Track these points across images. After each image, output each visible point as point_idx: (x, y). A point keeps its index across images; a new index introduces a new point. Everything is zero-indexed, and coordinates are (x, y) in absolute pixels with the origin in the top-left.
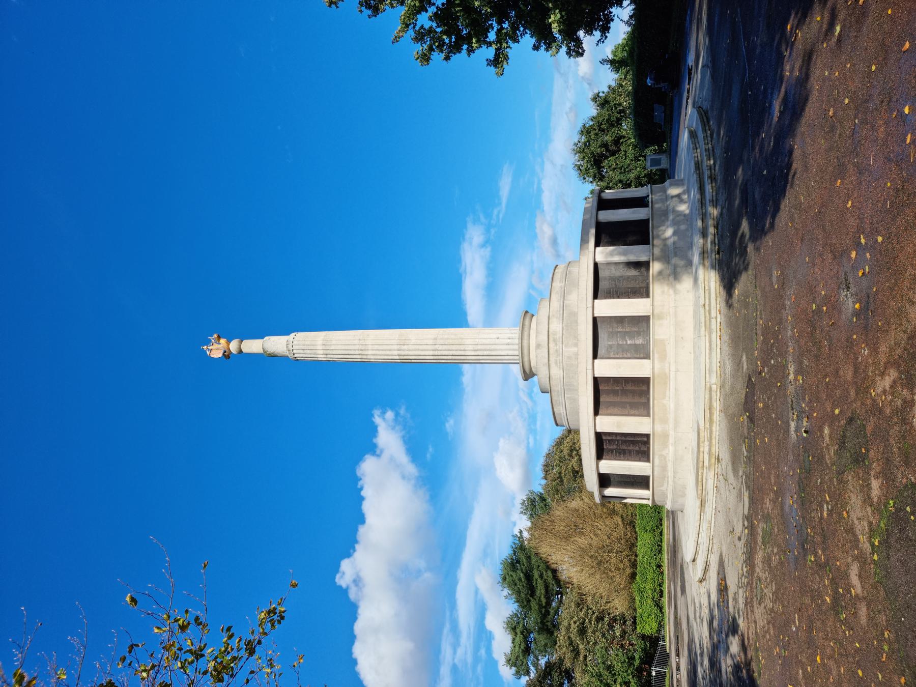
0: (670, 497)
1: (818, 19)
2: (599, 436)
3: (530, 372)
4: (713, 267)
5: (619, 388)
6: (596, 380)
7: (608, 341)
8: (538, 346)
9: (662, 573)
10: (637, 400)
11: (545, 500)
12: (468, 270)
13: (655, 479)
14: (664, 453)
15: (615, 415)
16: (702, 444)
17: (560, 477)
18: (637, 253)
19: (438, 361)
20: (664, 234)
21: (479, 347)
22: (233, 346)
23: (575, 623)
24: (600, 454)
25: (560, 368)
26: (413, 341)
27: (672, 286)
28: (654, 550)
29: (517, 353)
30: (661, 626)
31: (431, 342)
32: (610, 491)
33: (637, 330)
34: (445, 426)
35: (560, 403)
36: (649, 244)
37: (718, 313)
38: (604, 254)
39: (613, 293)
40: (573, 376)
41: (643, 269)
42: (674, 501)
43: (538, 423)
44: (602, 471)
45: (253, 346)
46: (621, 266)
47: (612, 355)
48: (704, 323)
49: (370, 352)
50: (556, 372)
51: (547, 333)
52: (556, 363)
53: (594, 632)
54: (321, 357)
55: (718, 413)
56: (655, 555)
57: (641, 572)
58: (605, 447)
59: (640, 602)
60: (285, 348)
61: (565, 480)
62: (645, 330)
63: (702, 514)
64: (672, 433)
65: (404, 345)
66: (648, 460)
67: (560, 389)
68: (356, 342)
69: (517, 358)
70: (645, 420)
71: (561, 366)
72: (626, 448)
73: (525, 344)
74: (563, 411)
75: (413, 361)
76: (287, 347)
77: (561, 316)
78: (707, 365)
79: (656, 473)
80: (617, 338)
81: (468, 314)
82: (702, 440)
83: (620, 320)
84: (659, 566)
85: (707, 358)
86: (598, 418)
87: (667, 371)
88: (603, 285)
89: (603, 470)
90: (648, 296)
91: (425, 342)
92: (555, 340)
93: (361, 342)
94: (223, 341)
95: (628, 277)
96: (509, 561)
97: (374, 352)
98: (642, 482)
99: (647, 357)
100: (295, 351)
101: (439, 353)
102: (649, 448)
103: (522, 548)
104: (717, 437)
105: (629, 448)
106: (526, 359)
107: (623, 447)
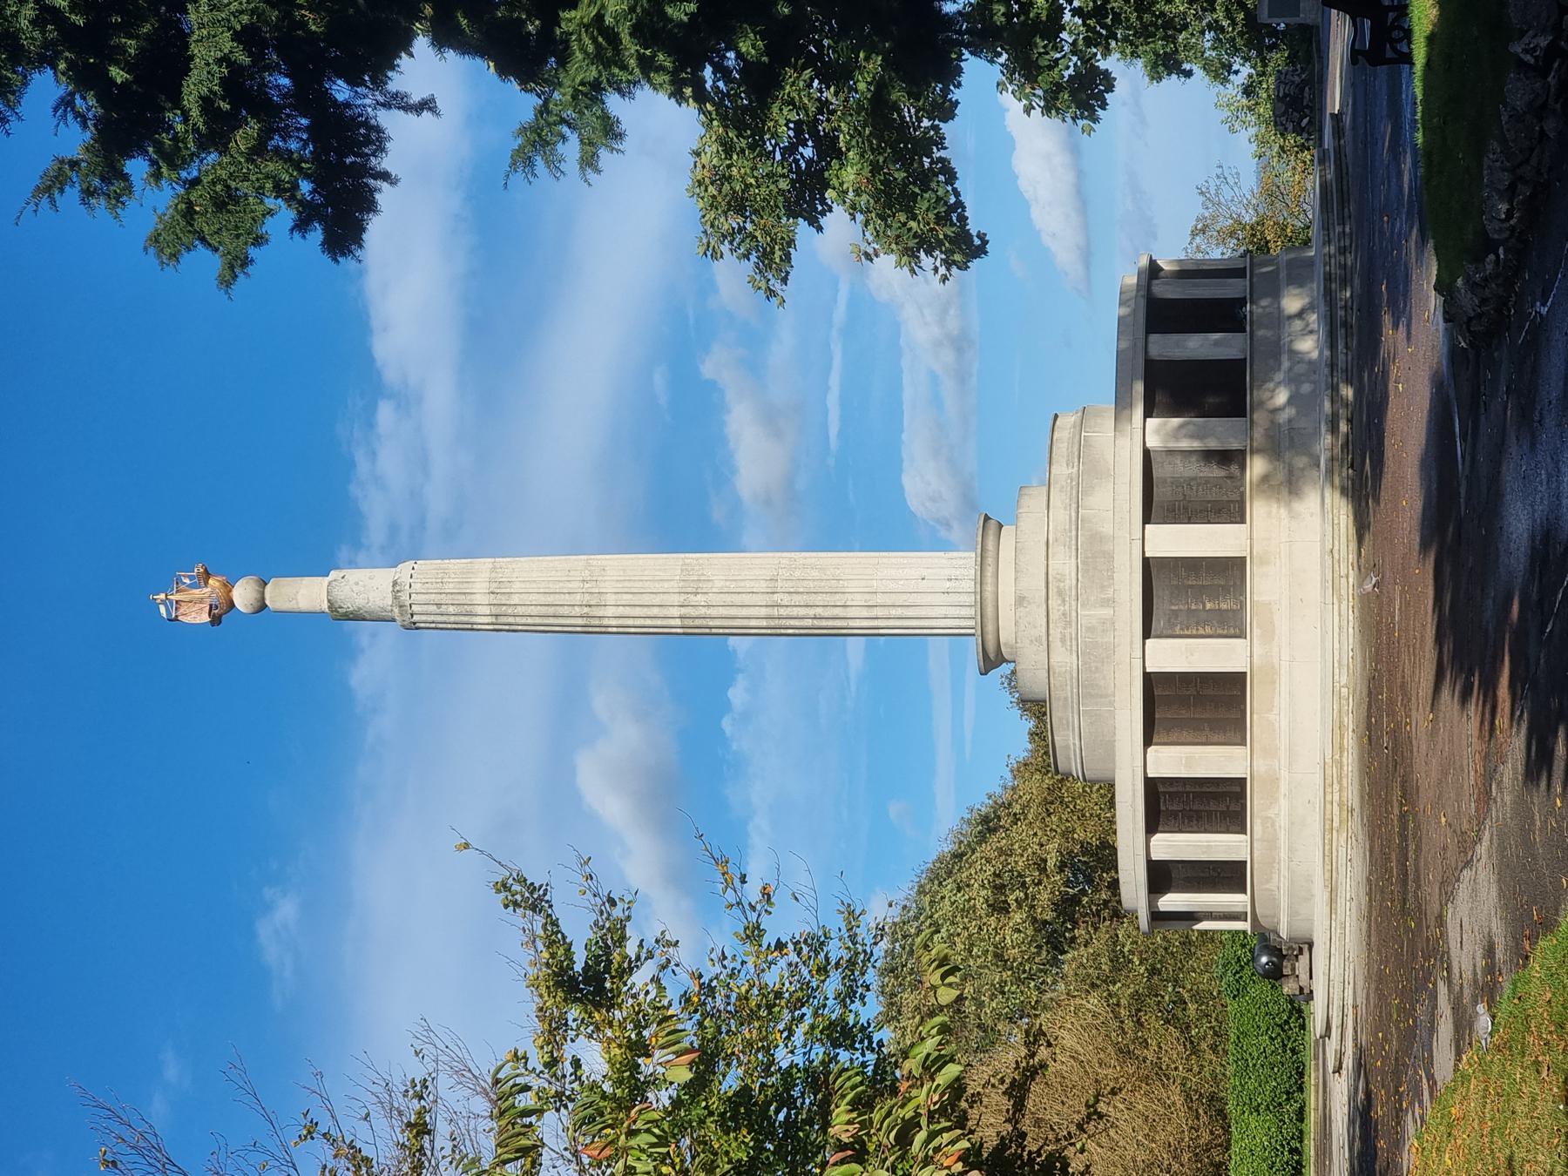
0: (1284, 904)
3: (997, 655)
4: (1344, 491)
6: (1149, 680)
8: (1020, 601)
13: (1256, 866)
14: (1271, 813)
18: (1222, 433)
19: (778, 631)
20: (1272, 397)
21: (880, 599)
24: (1154, 823)
25: (1071, 650)
26: (718, 584)
27: (1288, 505)
31: (762, 586)
32: (1172, 901)
35: (1068, 723)
36: (1245, 416)
37: (1350, 568)
38: (1159, 431)
39: (1179, 510)
40: (1097, 668)
42: (1293, 913)
46: (1194, 459)
48: (1331, 583)
49: (610, 611)
51: (1044, 576)
52: (1063, 641)
55: (1350, 733)
58: (1163, 808)
62: (1238, 583)
63: (1333, 916)
64: (1284, 773)
65: (696, 593)
67: (1069, 695)
68: (574, 586)
69: (972, 623)
71: (1074, 648)
72: (1202, 808)
73: (989, 595)
75: (714, 631)
76: (395, 598)
77: (1074, 542)
78: (1336, 653)
80: (1187, 597)
85: (1336, 641)
86: (1151, 750)
87: (1276, 661)
90: (1243, 521)
91: (748, 585)
92: (1060, 593)
93: (587, 586)
95: (1207, 481)
97: (621, 611)
98: (1229, 875)
99: (1241, 635)
101: (783, 612)
104: (1350, 774)
105: (1207, 808)
106: (990, 628)
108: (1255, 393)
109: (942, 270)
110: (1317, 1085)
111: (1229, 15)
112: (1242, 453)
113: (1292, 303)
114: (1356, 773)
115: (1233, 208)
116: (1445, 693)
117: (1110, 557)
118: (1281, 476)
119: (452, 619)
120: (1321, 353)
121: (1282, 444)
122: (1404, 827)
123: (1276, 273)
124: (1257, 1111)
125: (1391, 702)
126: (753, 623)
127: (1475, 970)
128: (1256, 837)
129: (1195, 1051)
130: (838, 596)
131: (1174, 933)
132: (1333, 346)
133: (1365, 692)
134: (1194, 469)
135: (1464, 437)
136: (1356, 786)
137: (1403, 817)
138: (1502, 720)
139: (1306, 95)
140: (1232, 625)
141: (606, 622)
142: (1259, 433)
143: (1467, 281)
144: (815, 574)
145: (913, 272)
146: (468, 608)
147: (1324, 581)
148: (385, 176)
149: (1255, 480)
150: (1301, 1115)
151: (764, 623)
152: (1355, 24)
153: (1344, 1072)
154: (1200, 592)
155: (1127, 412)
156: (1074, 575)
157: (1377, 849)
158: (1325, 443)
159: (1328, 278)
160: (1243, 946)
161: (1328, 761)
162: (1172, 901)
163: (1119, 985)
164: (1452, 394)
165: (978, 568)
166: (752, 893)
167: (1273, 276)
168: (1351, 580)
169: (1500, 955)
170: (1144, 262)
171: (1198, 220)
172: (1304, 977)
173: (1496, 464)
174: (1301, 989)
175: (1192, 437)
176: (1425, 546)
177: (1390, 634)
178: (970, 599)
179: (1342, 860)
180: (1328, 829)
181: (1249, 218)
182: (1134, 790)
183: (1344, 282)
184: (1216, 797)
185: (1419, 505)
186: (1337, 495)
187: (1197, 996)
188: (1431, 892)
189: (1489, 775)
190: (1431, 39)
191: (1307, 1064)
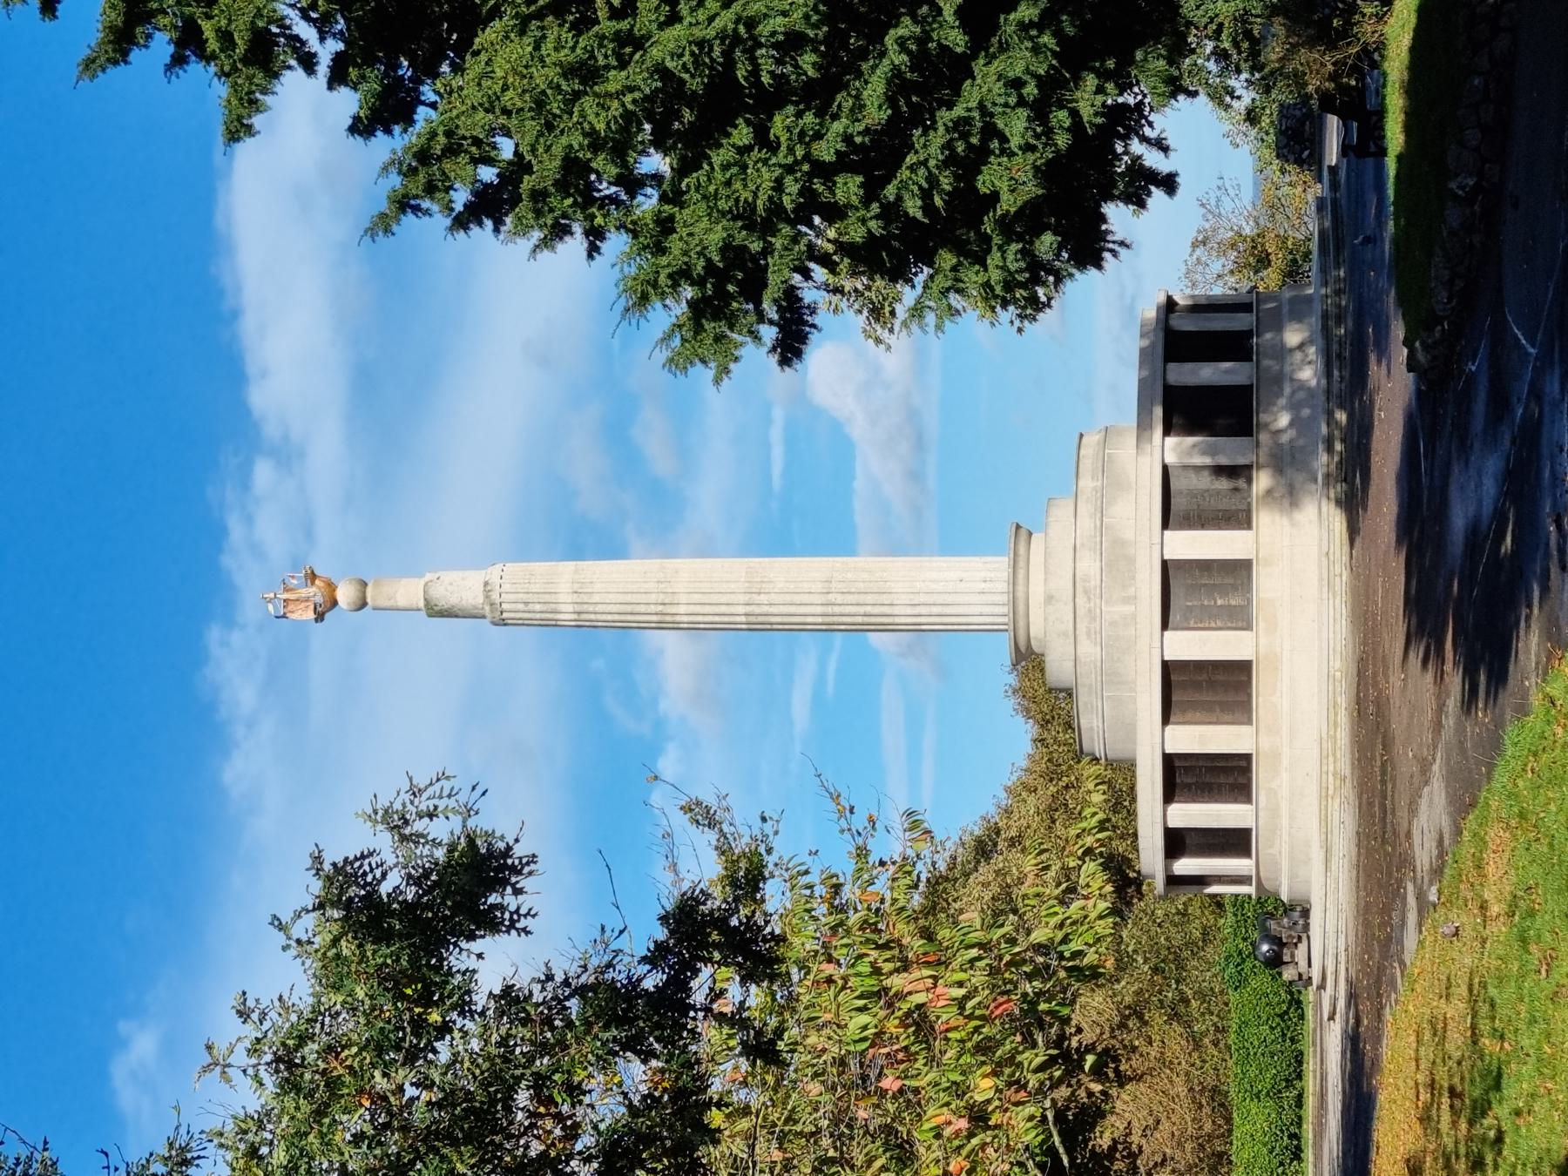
1: (1057, 1074)
2: (1170, 762)
4: (1338, 503)
6: (1167, 667)
7: (1187, 600)
8: (1049, 599)
13: (1260, 833)
15: (1196, 723)
16: (1325, 761)
18: (1232, 450)
21: (922, 599)
24: (1171, 793)
28: (1277, 1150)
31: (818, 587)
32: (1186, 866)
33: (1232, 581)
38: (1177, 449)
42: (1292, 877)
47: (1192, 624)
49: (682, 609)
52: (1088, 634)
56: (1281, 1164)
58: (1178, 780)
60: (480, 599)
68: (651, 586)
69: (1005, 620)
71: (1098, 640)
76: (487, 597)
78: (1331, 642)
79: (1260, 823)
82: (1325, 753)
83: (1206, 566)
86: (1169, 728)
89: (1173, 823)
90: (1248, 526)
91: (806, 587)
92: (1086, 592)
95: (1218, 492)
97: (692, 609)
99: (1248, 627)
100: (504, 606)
101: (837, 610)
102: (1250, 780)
106: (1021, 624)
107: (1208, 779)
108: (1261, 415)
109: (1017, 323)
110: (1314, 1071)
111: (1236, 44)
112: (1249, 467)
113: (1293, 336)
114: (1348, 744)
115: (1234, 220)
116: (1412, 655)
117: (1131, 561)
118: (1282, 490)
119: (538, 616)
120: (1318, 383)
121: (1287, 461)
122: (1384, 773)
123: (1278, 309)
124: (1258, 1098)
125: (1375, 674)
126: (810, 620)
127: (1471, 979)
128: (1261, 805)
129: (1198, 1046)
130: (885, 596)
131: (1183, 896)
132: (1328, 374)
133: (1355, 673)
134: (1205, 482)
135: (1426, 457)
136: (1348, 756)
137: (1383, 764)
138: (1448, 667)
139: (1307, 128)
140: (1240, 619)
141: (678, 618)
142: (1263, 452)
143: (1422, 344)
144: (865, 576)
145: (993, 324)
146: (553, 606)
147: (1321, 580)
148: (814, 326)
149: (1260, 493)
150: (1299, 1101)
151: (820, 620)
152: (1345, 125)
153: (1337, 1017)
154: (1212, 589)
155: (1146, 434)
156: (1098, 577)
157: (1364, 802)
158: (1322, 461)
159: (1325, 316)
160: (1245, 939)
161: (1324, 736)
162: (1186, 866)
163: (1123, 983)
164: (1419, 422)
165: (1011, 570)
166: (859, 822)
167: (1277, 312)
168: (1344, 578)
169: (1446, 842)
170: (1162, 298)
171: (1199, 232)
172: (1303, 964)
173: (1446, 477)
174: (1300, 975)
175: (1204, 453)
176: (1399, 542)
177: (1374, 620)
178: (1004, 598)
179: (1336, 822)
180: (1324, 796)
181: (1248, 230)
182: (1153, 765)
183: (1339, 319)
184: (1226, 771)
185: (1395, 509)
186: (1332, 505)
187: (1201, 995)
188: (1402, 814)
189: (1441, 708)
190: (1400, 158)
191: (1306, 1053)
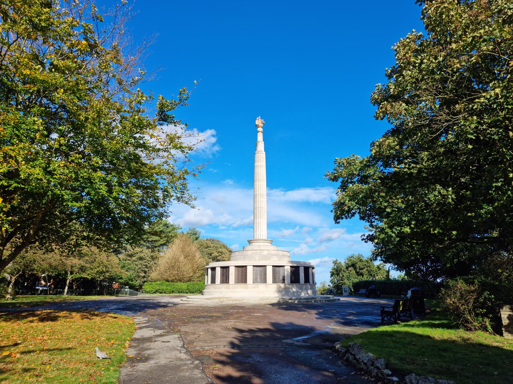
0: (209, 290)
2: (227, 268)
4: (279, 301)
5: (244, 274)
6: (246, 266)
8: (259, 246)
9: (170, 293)
10: (240, 279)
11: (196, 240)
12: (318, 191)
17: (208, 247)
18: (288, 280)
21: (259, 224)
22: (260, 129)
23: (144, 255)
24: (222, 268)
29: (257, 238)
30: (147, 292)
31: (261, 206)
34: (229, 179)
41: (282, 281)
42: (207, 292)
43: (233, 232)
44: (216, 268)
45: (260, 137)
49: (258, 183)
50: (250, 253)
53: (141, 264)
54: (256, 164)
57: (170, 284)
59: (158, 284)
61: (207, 250)
66: (220, 283)
70: (234, 282)
74: (237, 255)
81: (292, 191)
83: (265, 274)
84: (173, 292)
88: (277, 268)
92: (260, 252)
94: (262, 125)
95: (280, 277)
96: (168, 223)
98: (213, 281)
99: (253, 283)
103: (174, 229)
106: (255, 241)
